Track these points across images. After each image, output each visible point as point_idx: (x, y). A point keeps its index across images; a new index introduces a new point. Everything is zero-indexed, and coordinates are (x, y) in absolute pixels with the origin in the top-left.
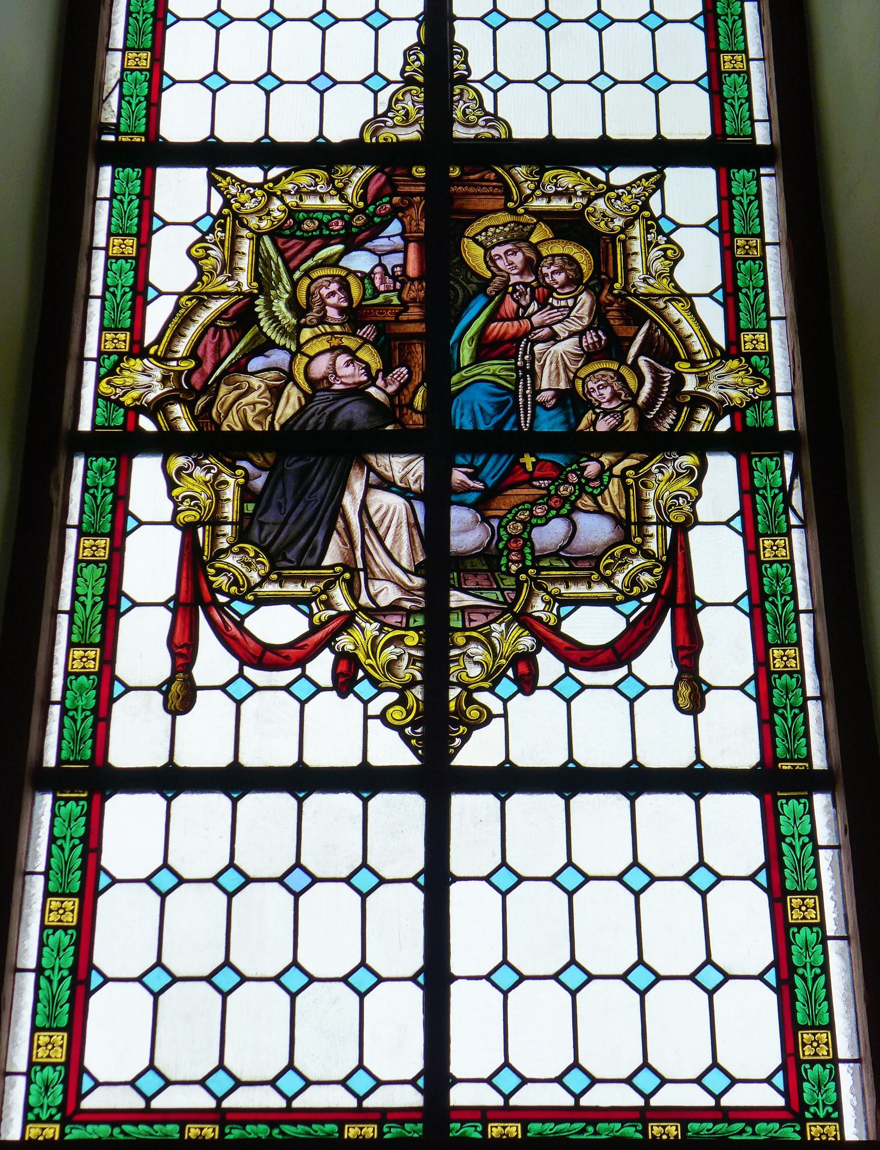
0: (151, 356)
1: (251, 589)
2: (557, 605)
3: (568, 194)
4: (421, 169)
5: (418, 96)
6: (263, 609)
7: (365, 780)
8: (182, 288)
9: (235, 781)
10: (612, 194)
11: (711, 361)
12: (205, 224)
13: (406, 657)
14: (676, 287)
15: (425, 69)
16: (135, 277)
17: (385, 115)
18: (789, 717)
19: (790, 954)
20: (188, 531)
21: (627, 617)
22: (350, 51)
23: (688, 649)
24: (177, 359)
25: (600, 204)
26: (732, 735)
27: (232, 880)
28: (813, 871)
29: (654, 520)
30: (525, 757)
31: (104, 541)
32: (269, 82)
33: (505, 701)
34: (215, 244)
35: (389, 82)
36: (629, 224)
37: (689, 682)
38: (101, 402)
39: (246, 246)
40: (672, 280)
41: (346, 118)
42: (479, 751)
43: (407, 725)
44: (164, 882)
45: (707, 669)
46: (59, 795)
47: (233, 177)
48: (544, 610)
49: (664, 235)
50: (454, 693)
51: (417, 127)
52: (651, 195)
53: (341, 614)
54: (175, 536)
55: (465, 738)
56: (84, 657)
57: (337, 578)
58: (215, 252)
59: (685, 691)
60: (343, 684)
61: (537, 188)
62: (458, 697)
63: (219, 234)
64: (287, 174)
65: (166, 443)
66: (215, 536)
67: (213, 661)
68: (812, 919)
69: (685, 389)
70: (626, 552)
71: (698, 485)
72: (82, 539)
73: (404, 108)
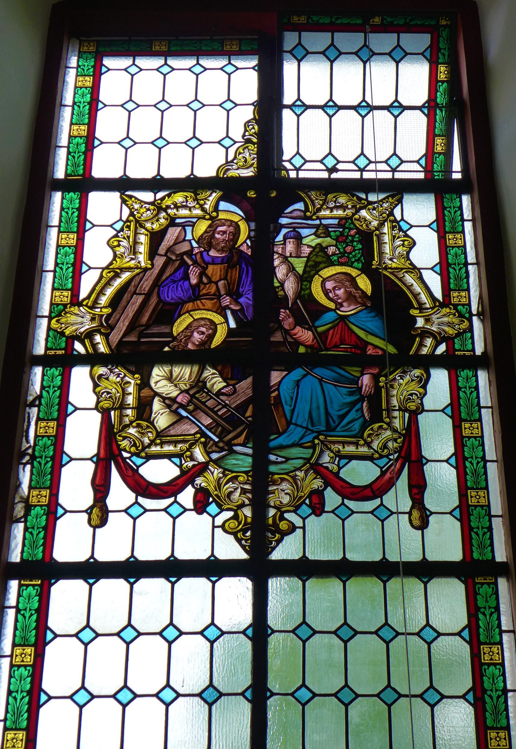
0: (84, 305)
1: (144, 448)
2: (337, 459)
3: (343, 207)
4: (252, 193)
5: (253, 150)
6: (151, 462)
7: (212, 569)
8: (104, 265)
9: (132, 570)
10: (370, 207)
11: (432, 308)
12: (118, 226)
13: (239, 490)
14: (412, 264)
15: (258, 135)
16: (75, 258)
17: (232, 161)
18: (481, 534)
19: (482, 682)
20: (105, 413)
21: (381, 468)
22: (212, 124)
23: (418, 487)
24: (101, 308)
25: (363, 213)
26: (445, 541)
27: (129, 633)
28: (484, 477)
29: (397, 408)
30: (315, 554)
31: (53, 423)
32: (160, 143)
33: (304, 519)
34: (124, 238)
35: (235, 142)
36: (381, 224)
37: (419, 510)
38: (51, 333)
39: (143, 239)
40: (408, 259)
41: (208, 166)
42: (286, 550)
43: (239, 531)
44: (87, 634)
45: (430, 502)
46: (22, 582)
47: (136, 198)
48: (329, 462)
49: (403, 232)
50: (272, 512)
51: (252, 169)
52: (394, 208)
53: (200, 463)
54: (97, 417)
55: (279, 542)
56: (39, 495)
57: (197, 441)
58: (124, 243)
59: (416, 514)
60: (200, 507)
61: (324, 204)
62: (274, 516)
63: (126, 232)
64: (169, 196)
65: (92, 359)
66: (121, 417)
67: (120, 494)
68: (503, 746)
69: (417, 326)
70: (380, 427)
71: (424, 387)
72: (39, 422)
73: (244, 157)
